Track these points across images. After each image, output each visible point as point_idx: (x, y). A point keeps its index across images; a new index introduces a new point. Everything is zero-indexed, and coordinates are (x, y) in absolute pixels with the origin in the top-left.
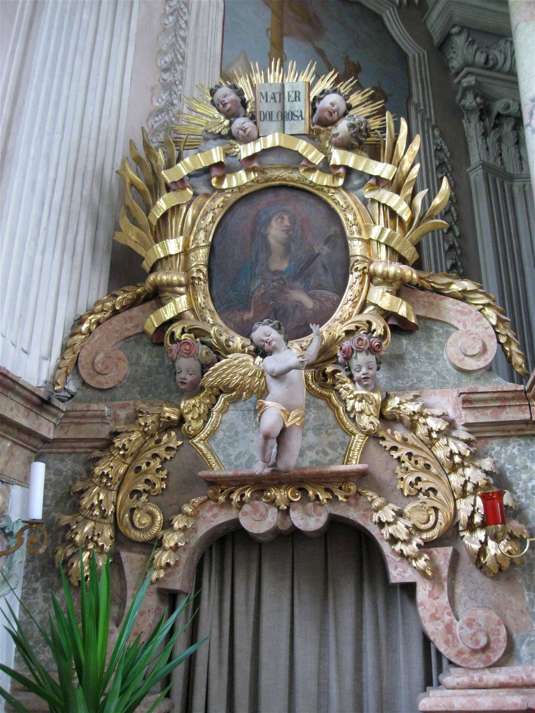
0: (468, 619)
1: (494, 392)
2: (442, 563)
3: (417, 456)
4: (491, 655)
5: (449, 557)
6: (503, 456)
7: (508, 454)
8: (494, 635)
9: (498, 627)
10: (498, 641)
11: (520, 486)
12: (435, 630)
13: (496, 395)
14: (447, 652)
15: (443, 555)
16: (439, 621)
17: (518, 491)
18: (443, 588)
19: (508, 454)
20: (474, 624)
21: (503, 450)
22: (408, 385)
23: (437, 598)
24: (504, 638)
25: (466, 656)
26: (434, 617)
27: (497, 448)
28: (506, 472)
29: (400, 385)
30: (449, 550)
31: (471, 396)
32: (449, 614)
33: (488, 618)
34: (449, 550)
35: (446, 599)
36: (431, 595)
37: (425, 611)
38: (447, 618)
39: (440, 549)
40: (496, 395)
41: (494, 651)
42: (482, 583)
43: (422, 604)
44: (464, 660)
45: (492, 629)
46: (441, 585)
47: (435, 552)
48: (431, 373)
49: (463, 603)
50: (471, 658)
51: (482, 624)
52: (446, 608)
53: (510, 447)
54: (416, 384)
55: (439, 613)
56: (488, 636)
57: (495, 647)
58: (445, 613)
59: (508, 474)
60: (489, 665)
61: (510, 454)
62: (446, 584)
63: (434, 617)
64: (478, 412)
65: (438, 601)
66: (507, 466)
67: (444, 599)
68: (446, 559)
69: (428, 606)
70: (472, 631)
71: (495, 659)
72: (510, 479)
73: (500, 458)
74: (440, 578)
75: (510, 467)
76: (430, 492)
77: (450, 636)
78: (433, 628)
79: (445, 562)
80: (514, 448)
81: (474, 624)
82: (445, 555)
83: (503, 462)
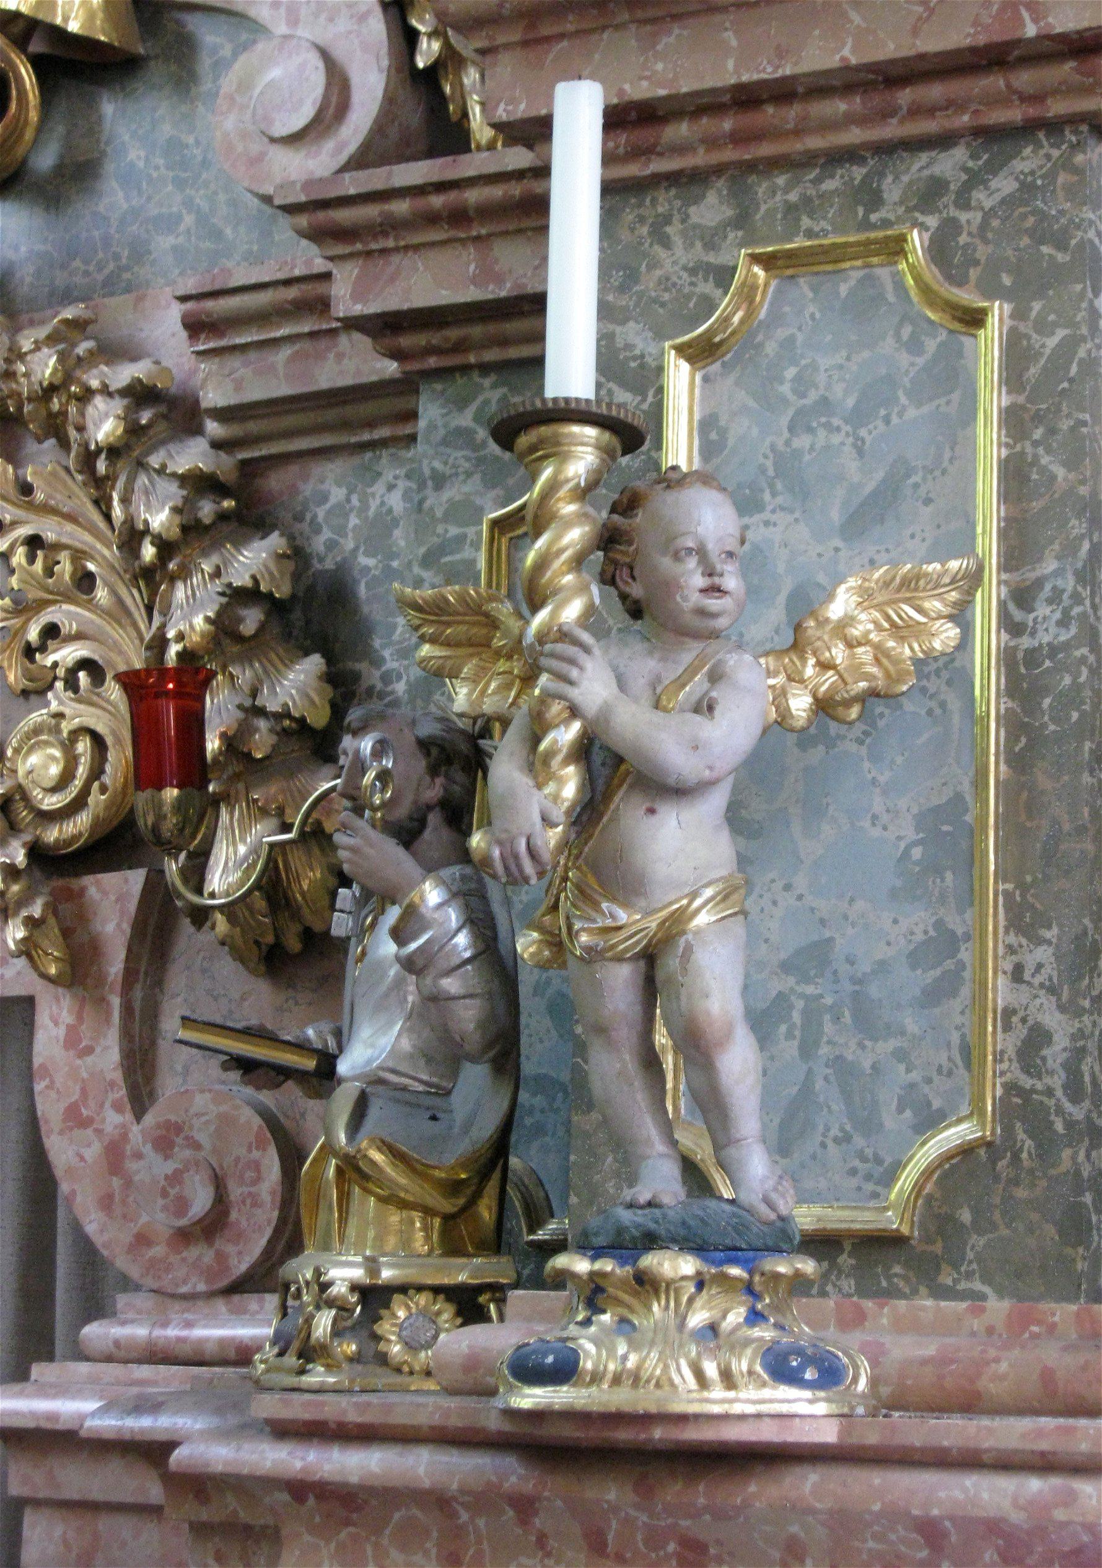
0: (158, 1126)
1: (288, 282)
2: (110, 928)
3: (57, 547)
4: (230, 1249)
5: (132, 906)
6: (354, 521)
7: (371, 513)
8: (241, 1180)
9: (256, 1154)
10: (255, 1204)
11: (396, 637)
12: (74, 1161)
13: (292, 293)
14: (106, 1237)
15: (113, 899)
16: (89, 1132)
17: (386, 654)
18: (108, 1020)
19: (371, 513)
20: (179, 1140)
21: (355, 500)
22: (100, 277)
23: (89, 1050)
24: (273, 1193)
25: (158, 1251)
26: (76, 1118)
27: (337, 494)
28: (356, 582)
29: (78, 279)
30: (134, 880)
31: (210, 304)
32: (118, 1108)
33: (226, 1122)
34: (134, 880)
35: (114, 1055)
36: (72, 1040)
37: (53, 1094)
38: (113, 1120)
39: (111, 880)
40: (292, 293)
41: (239, 1237)
42: (243, 999)
43: (45, 1070)
44: (152, 1265)
45: (237, 1160)
46: (101, 1002)
47: (92, 891)
48: (179, 218)
49: (179, 1068)
50: (174, 1259)
51: (203, 1138)
52: (112, 1084)
53: (379, 488)
54: (127, 268)
55: (92, 1103)
56: (219, 1183)
57: (244, 1223)
58: (108, 1104)
59: (362, 591)
60: (224, 1282)
61: (378, 514)
62: (116, 1001)
63: (76, 1118)
64: (246, 365)
65: (89, 1060)
66: (364, 560)
67: (108, 1056)
68: (122, 912)
69: (59, 1080)
70: (170, 1167)
71: (241, 1265)
72: (366, 609)
73: (341, 531)
74: (101, 981)
75: (371, 562)
76: (82, 675)
77: (116, 1182)
78: (70, 1153)
79: (119, 925)
80: (391, 487)
81: (179, 1140)
82: (121, 898)
83: (350, 545)
